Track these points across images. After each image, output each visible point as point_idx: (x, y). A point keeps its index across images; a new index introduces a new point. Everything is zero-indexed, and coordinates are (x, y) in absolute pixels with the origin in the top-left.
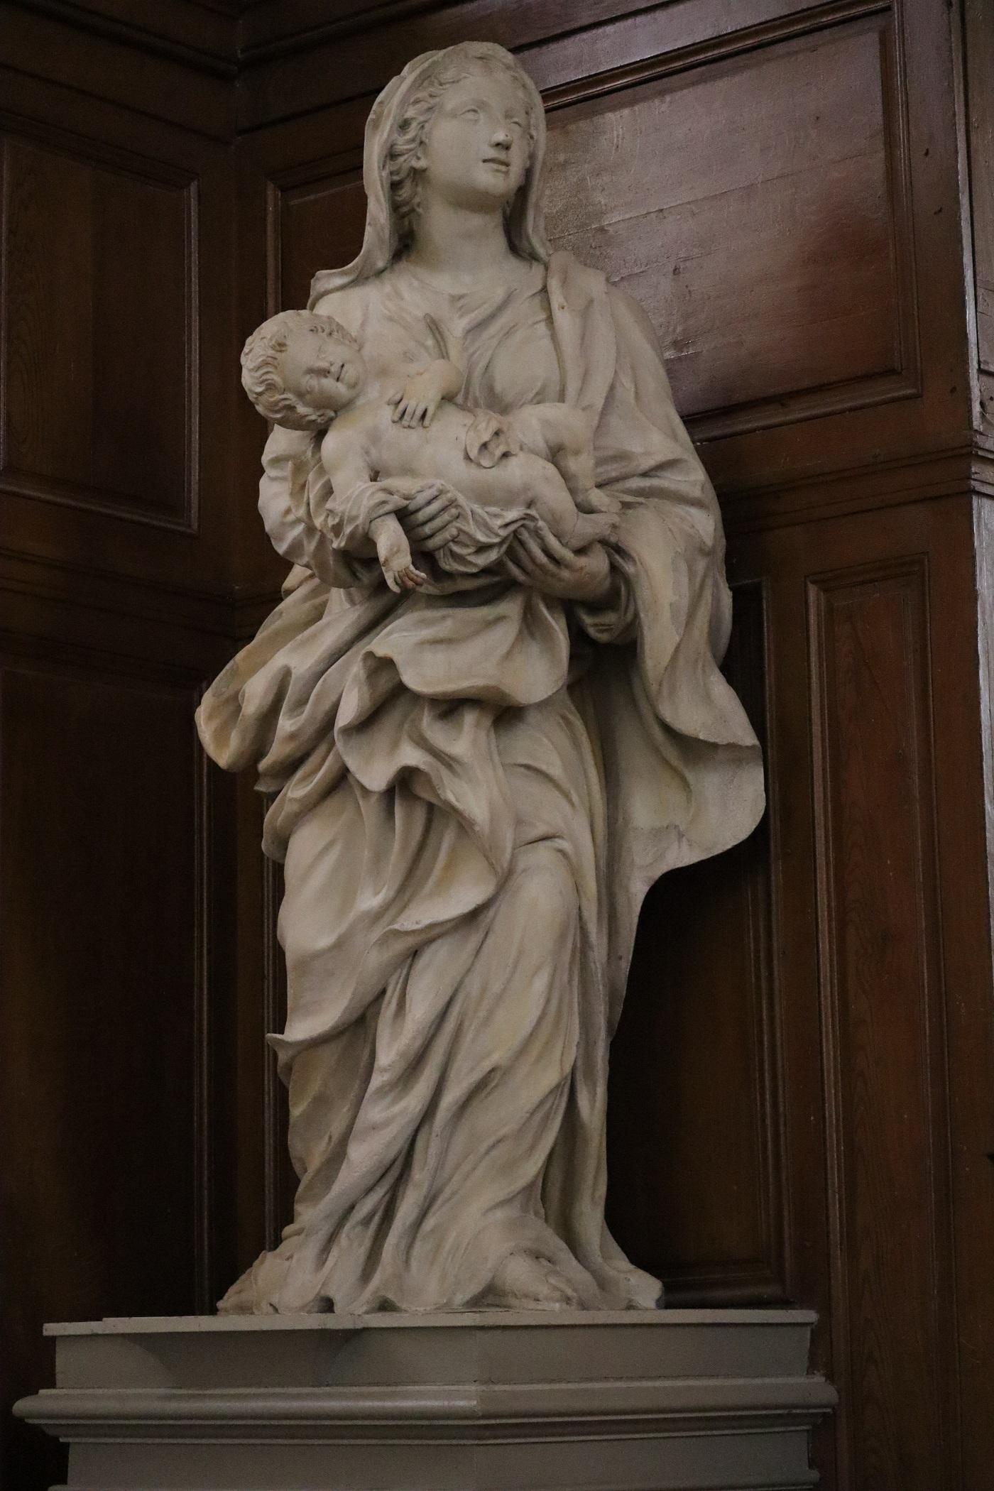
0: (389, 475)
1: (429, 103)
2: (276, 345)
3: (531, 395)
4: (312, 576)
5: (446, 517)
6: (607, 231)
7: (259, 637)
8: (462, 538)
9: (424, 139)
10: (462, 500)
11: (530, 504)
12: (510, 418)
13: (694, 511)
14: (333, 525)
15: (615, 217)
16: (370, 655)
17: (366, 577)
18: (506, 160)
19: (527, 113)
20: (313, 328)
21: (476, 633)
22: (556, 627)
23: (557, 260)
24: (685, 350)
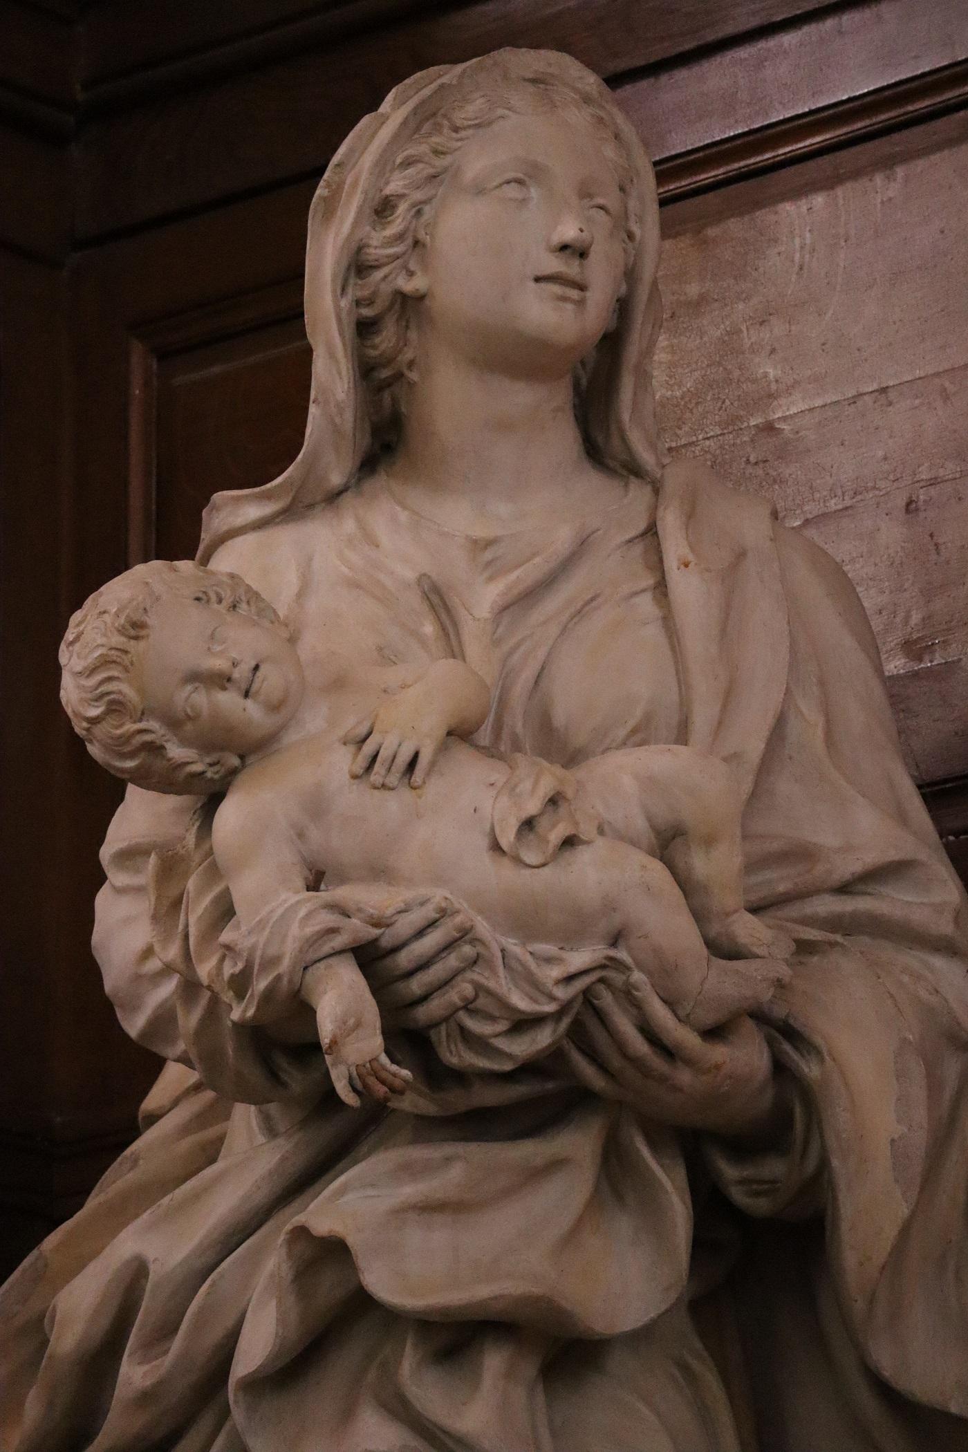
0: (343, 879)
1: (434, 167)
2: (128, 627)
3: (622, 733)
4: (197, 1088)
5: (452, 961)
6: (780, 431)
7: (92, 1203)
8: (482, 1002)
9: (421, 235)
10: (483, 928)
11: (615, 940)
12: (580, 773)
13: (939, 962)
14: (232, 975)
15: (793, 405)
16: (301, 1232)
17: (297, 1081)
18: (578, 278)
19: (622, 189)
20: (200, 595)
21: (508, 1193)
22: (668, 1185)
23: (675, 478)
24: (927, 658)
